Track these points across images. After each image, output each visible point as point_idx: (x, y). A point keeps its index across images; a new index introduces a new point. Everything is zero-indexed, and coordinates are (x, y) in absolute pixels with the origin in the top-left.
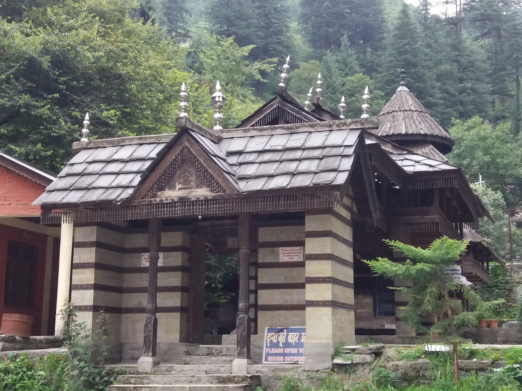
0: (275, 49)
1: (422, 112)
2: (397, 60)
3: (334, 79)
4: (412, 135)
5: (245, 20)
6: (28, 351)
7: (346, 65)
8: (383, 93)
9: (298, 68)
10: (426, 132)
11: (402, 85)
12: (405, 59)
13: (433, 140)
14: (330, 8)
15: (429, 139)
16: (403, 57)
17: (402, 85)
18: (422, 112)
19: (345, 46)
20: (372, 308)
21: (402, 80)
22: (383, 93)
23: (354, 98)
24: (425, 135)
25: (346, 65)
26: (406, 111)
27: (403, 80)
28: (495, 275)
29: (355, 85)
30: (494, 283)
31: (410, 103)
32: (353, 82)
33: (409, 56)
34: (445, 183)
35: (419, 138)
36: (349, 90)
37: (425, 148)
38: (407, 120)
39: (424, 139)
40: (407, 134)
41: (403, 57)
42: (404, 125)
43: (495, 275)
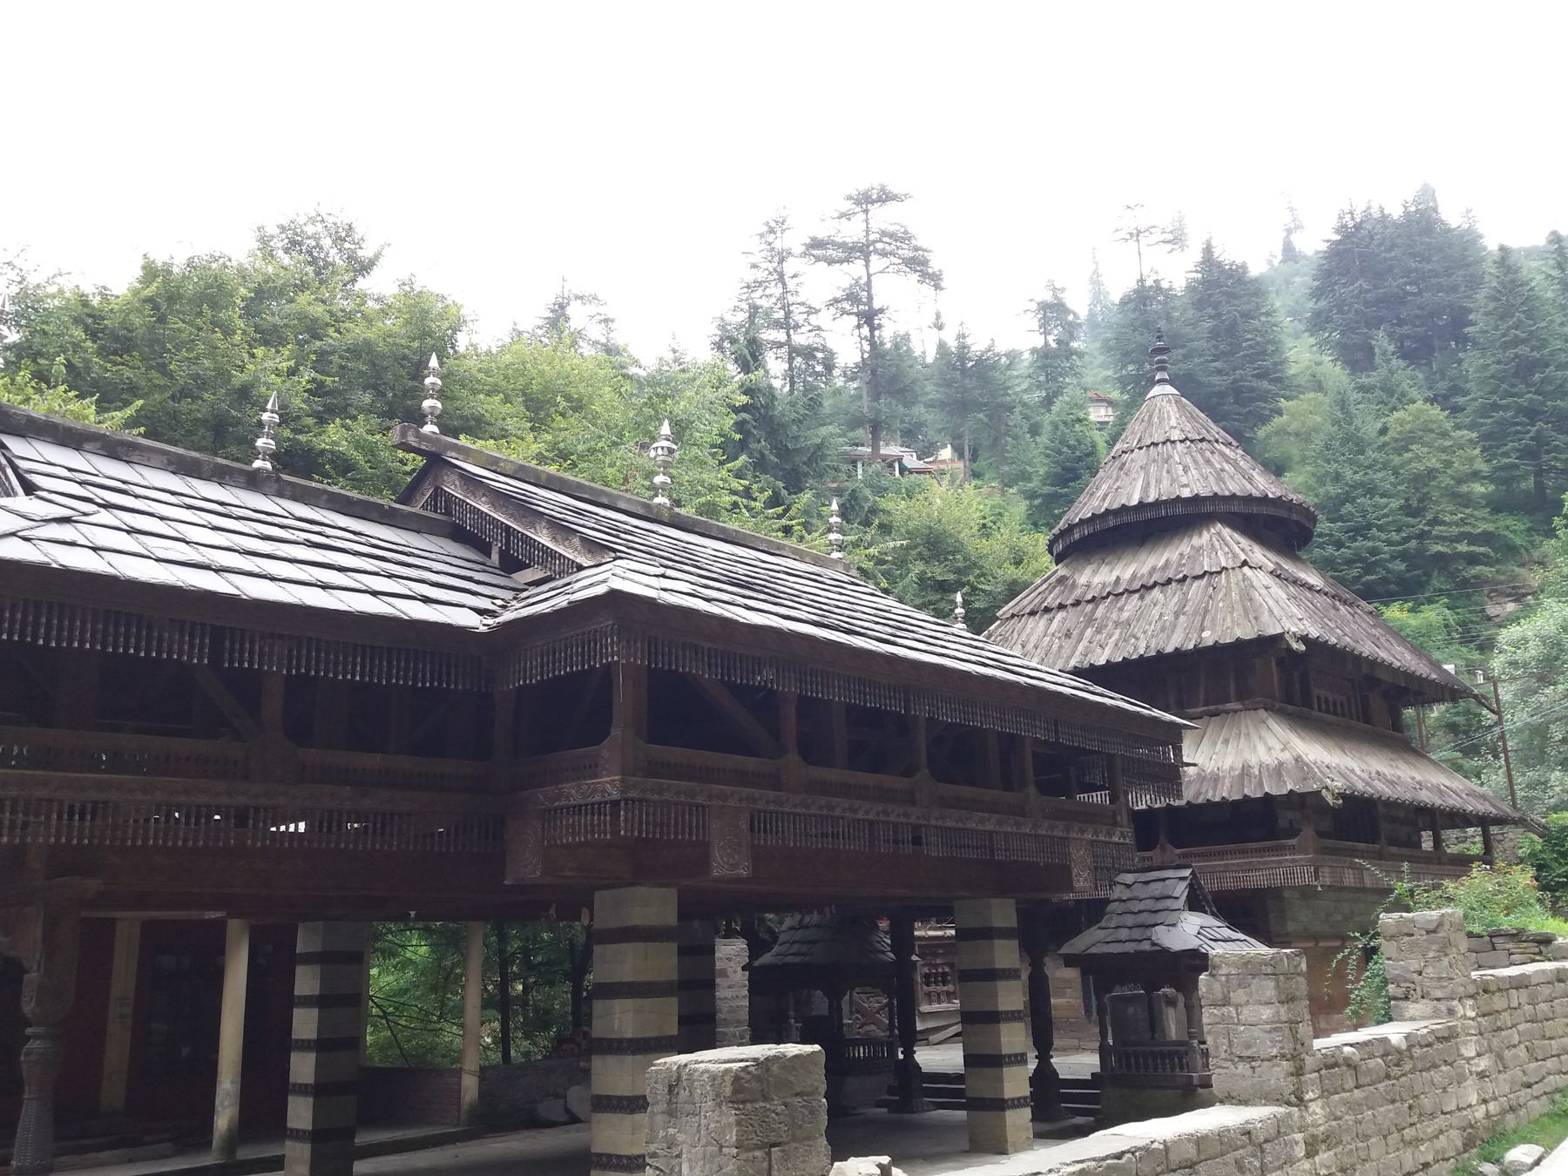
0: (1252, 390)
1: (1202, 440)
2: (1499, 363)
3: (1357, 422)
4: (1157, 504)
5: (1183, 346)
6: (683, 1058)
7: (1391, 393)
8: (1475, 435)
9: (1281, 414)
10: (1216, 489)
11: (1160, 381)
12: (1516, 356)
13: (1222, 508)
14: (1368, 291)
15: (1210, 508)
16: (1511, 353)
17: (1160, 381)
18: (1202, 440)
19: (1384, 353)
20: (1079, 994)
21: (1159, 369)
22: (1475, 435)
23: (1408, 455)
24: (1196, 499)
25: (1391, 393)
26: (1156, 445)
27: (1163, 369)
28: (1559, 852)
29: (1408, 427)
30: (1559, 876)
31: (1173, 422)
32: (1401, 422)
33: (1523, 350)
34: (192, 646)
35: (1179, 510)
36: (1396, 440)
37: (1200, 535)
38: (1153, 468)
39: (1191, 510)
40: (1142, 505)
41: (1511, 353)
42: (1140, 483)
43: (1559, 852)
